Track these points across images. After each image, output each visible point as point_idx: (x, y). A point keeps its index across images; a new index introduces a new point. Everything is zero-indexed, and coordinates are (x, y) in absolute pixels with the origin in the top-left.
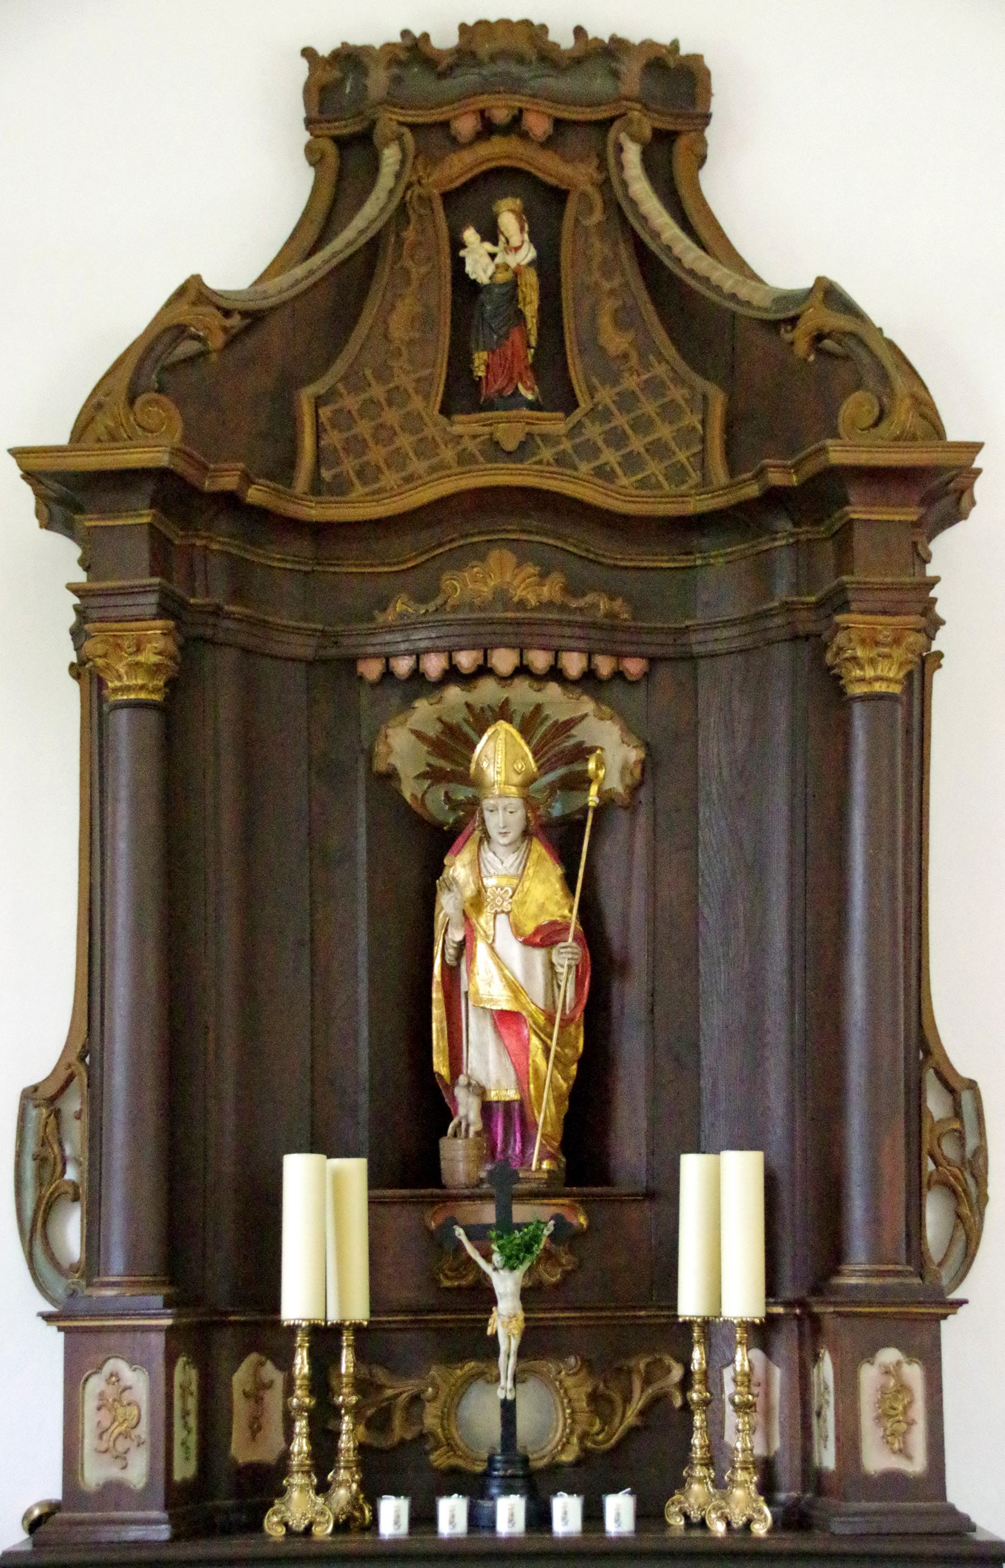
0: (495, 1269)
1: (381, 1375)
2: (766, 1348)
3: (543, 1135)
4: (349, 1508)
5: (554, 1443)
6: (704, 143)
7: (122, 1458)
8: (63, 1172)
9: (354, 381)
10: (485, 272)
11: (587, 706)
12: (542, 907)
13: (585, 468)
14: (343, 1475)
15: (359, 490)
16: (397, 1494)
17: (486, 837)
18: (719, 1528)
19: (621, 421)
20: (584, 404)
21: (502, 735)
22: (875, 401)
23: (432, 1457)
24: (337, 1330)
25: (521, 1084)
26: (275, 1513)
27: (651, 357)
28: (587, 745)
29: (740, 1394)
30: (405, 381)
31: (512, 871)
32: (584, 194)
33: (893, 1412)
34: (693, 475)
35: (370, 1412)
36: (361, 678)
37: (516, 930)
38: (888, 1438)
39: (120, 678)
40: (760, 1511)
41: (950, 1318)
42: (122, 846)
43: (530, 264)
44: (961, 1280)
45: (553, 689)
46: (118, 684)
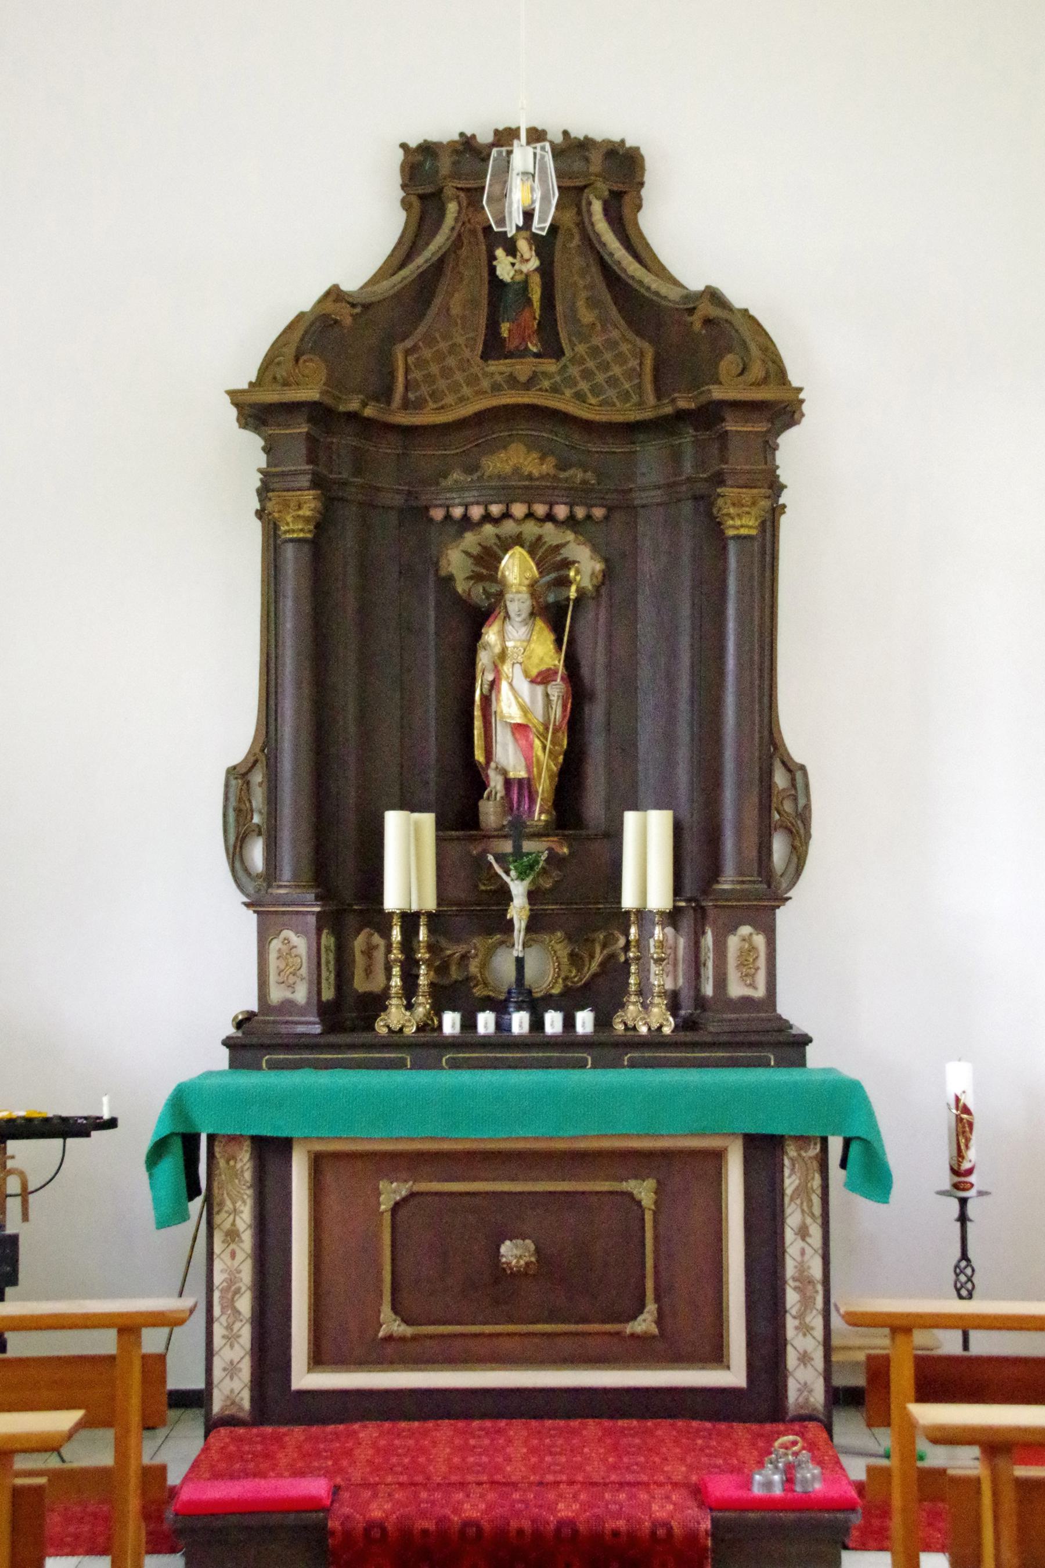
0: (512, 880)
1: (443, 942)
2: (676, 928)
3: (542, 799)
4: (425, 1018)
5: (548, 983)
6: (640, 198)
7: (292, 987)
8: (252, 818)
9: (429, 340)
10: (508, 274)
11: (570, 536)
12: (542, 659)
13: (568, 393)
14: (421, 999)
15: (432, 405)
16: (454, 1010)
17: (507, 616)
18: (643, 1030)
19: (591, 364)
20: (568, 353)
21: (517, 556)
22: (740, 360)
23: (474, 991)
24: (417, 915)
25: (529, 768)
26: (381, 1020)
27: (609, 325)
28: (570, 559)
29: (657, 953)
30: (460, 340)
31: (523, 638)
32: (569, 230)
33: (746, 963)
34: (634, 396)
35: (438, 963)
36: (431, 520)
37: (526, 674)
38: (744, 977)
39: (288, 524)
40: (667, 1020)
41: (781, 907)
42: (288, 625)
43: (537, 270)
44: (794, 885)
45: (549, 526)
46: (286, 528)
